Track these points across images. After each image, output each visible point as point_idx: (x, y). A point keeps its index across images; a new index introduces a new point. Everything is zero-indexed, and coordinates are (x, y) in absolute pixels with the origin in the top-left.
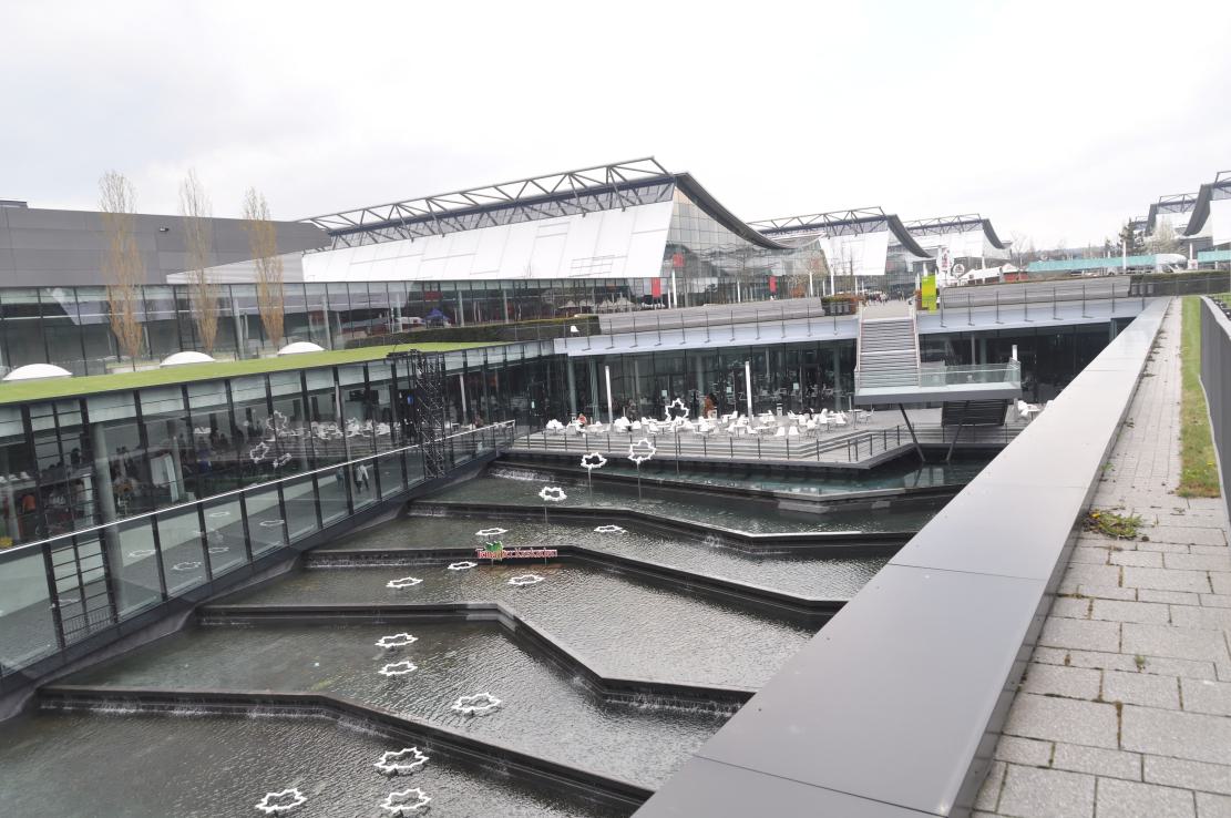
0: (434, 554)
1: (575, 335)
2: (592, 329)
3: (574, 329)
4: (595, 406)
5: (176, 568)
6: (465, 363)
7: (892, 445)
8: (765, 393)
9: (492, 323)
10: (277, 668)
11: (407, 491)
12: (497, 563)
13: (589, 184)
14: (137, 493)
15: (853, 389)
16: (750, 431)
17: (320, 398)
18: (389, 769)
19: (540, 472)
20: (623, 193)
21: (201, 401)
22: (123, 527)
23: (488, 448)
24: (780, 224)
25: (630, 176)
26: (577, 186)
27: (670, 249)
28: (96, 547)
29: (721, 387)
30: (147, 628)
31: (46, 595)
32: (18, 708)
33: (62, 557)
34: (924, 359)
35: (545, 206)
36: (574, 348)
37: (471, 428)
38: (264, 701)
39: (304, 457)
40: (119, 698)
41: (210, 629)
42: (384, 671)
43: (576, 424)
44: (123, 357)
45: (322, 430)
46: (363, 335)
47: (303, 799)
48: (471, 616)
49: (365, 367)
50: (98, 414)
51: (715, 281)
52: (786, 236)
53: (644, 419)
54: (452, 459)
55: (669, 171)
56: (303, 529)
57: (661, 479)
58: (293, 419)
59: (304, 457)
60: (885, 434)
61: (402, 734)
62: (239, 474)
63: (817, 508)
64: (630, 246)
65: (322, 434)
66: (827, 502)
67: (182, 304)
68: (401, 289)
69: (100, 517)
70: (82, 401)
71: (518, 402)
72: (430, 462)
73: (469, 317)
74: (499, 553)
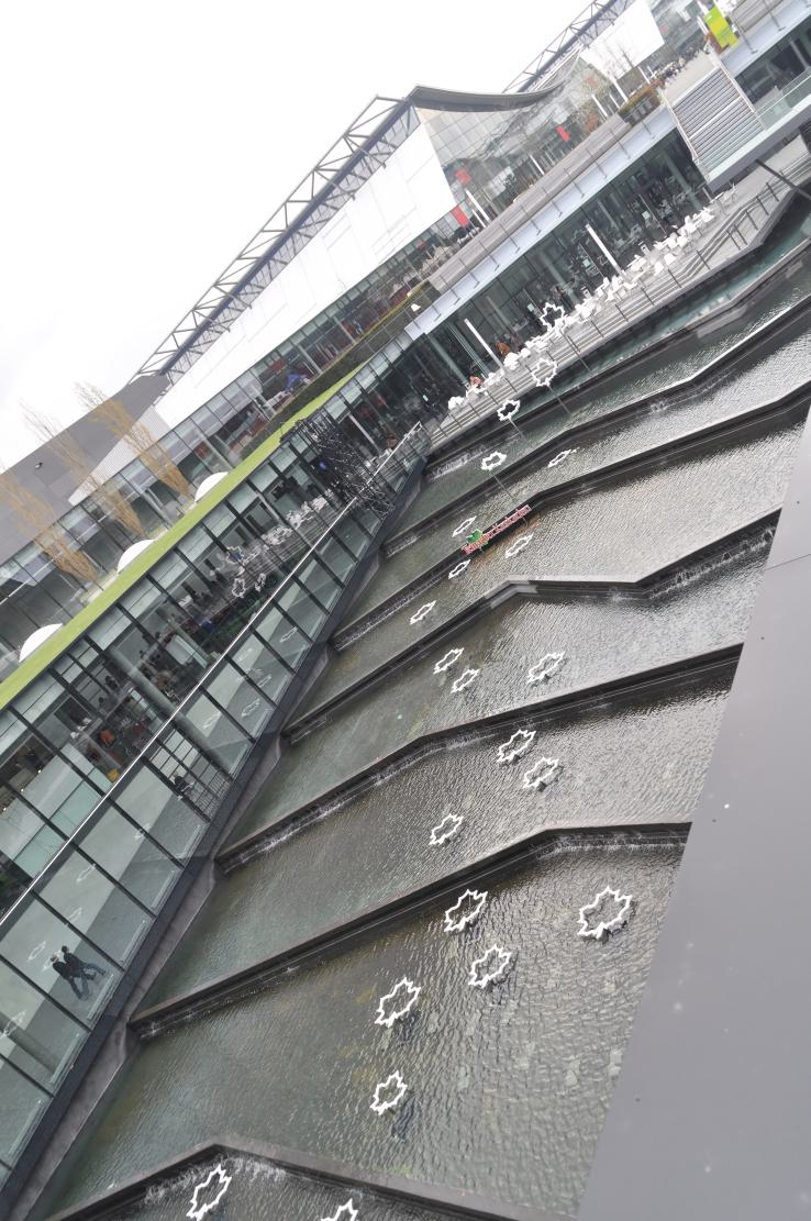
0: (427, 577)
1: (420, 311)
2: (431, 295)
3: (415, 307)
4: (478, 361)
5: (243, 715)
6: (346, 403)
7: (772, 205)
8: (621, 242)
11: (374, 540)
12: (485, 548)
13: (338, 165)
15: (701, 179)
16: (629, 286)
18: (511, 757)
19: (470, 450)
20: (374, 150)
21: (168, 578)
23: (414, 461)
24: (533, 70)
25: (369, 129)
26: (330, 175)
27: (449, 171)
28: (177, 737)
29: (578, 265)
30: (256, 770)
32: (212, 881)
33: (159, 759)
34: (754, 98)
35: (315, 215)
36: (427, 324)
38: (381, 767)
42: (455, 689)
43: (473, 390)
45: (273, 538)
46: (248, 439)
47: (461, 819)
48: (494, 604)
50: (104, 641)
51: (509, 171)
52: (547, 77)
53: (528, 343)
54: (391, 489)
55: (399, 97)
57: (576, 385)
58: (245, 545)
59: (275, 568)
60: (758, 200)
61: (501, 727)
62: (238, 613)
63: (736, 314)
64: (411, 196)
65: (275, 541)
66: (741, 302)
67: (96, 515)
69: (164, 714)
70: (86, 638)
71: (413, 404)
73: (321, 361)
74: (482, 539)
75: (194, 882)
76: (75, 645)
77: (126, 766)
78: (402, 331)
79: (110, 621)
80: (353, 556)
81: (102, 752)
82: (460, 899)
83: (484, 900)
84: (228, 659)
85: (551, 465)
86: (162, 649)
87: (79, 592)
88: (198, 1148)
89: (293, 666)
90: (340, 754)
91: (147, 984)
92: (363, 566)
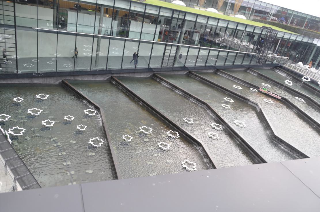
0: (248, 83)
5: (189, 60)
6: (283, 36)
9: (298, 27)
10: (200, 93)
11: (250, 65)
12: (263, 93)
14: (188, 40)
17: (239, 32)
18: (213, 127)
19: (289, 75)
21: (211, 23)
22: (183, 46)
23: (277, 63)
28: (175, 48)
31: (162, 55)
33: (168, 48)
37: (276, 55)
38: (194, 98)
39: (228, 46)
40: (168, 83)
41: (190, 77)
42: (223, 105)
43: (307, 66)
44: (198, 5)
45: (236, 41)
46: (259, 18)
47: (193, 123)
48: (250, 103)
49: (255, 28)
50: (187, 18)
54: (266, 62)
56: (220, 63)
59: (228, 46)
61: (220, 121)
62: (212, 44)
65: (235, 42)
68: (275, 8)
70: (186, 13)
71: (293, 53)
72: (259, 60)
73: (292, 23)
74: (265, 91)
75: (147, 72)
76: (182, 12)
77: (163, 41)
78: (314, 39)
79: (191, 16)
80: (242, 62)
81: (163, 34)
82: (175, 132)
83: (177, 137)
84: (200, 49)
85: (297, 98)
86: (193, 32)
87: (196, 4)
88: (97, 105)
89: (207, 64)
90: (193, 87)
91: (121, 75)
92: (241, 66)
